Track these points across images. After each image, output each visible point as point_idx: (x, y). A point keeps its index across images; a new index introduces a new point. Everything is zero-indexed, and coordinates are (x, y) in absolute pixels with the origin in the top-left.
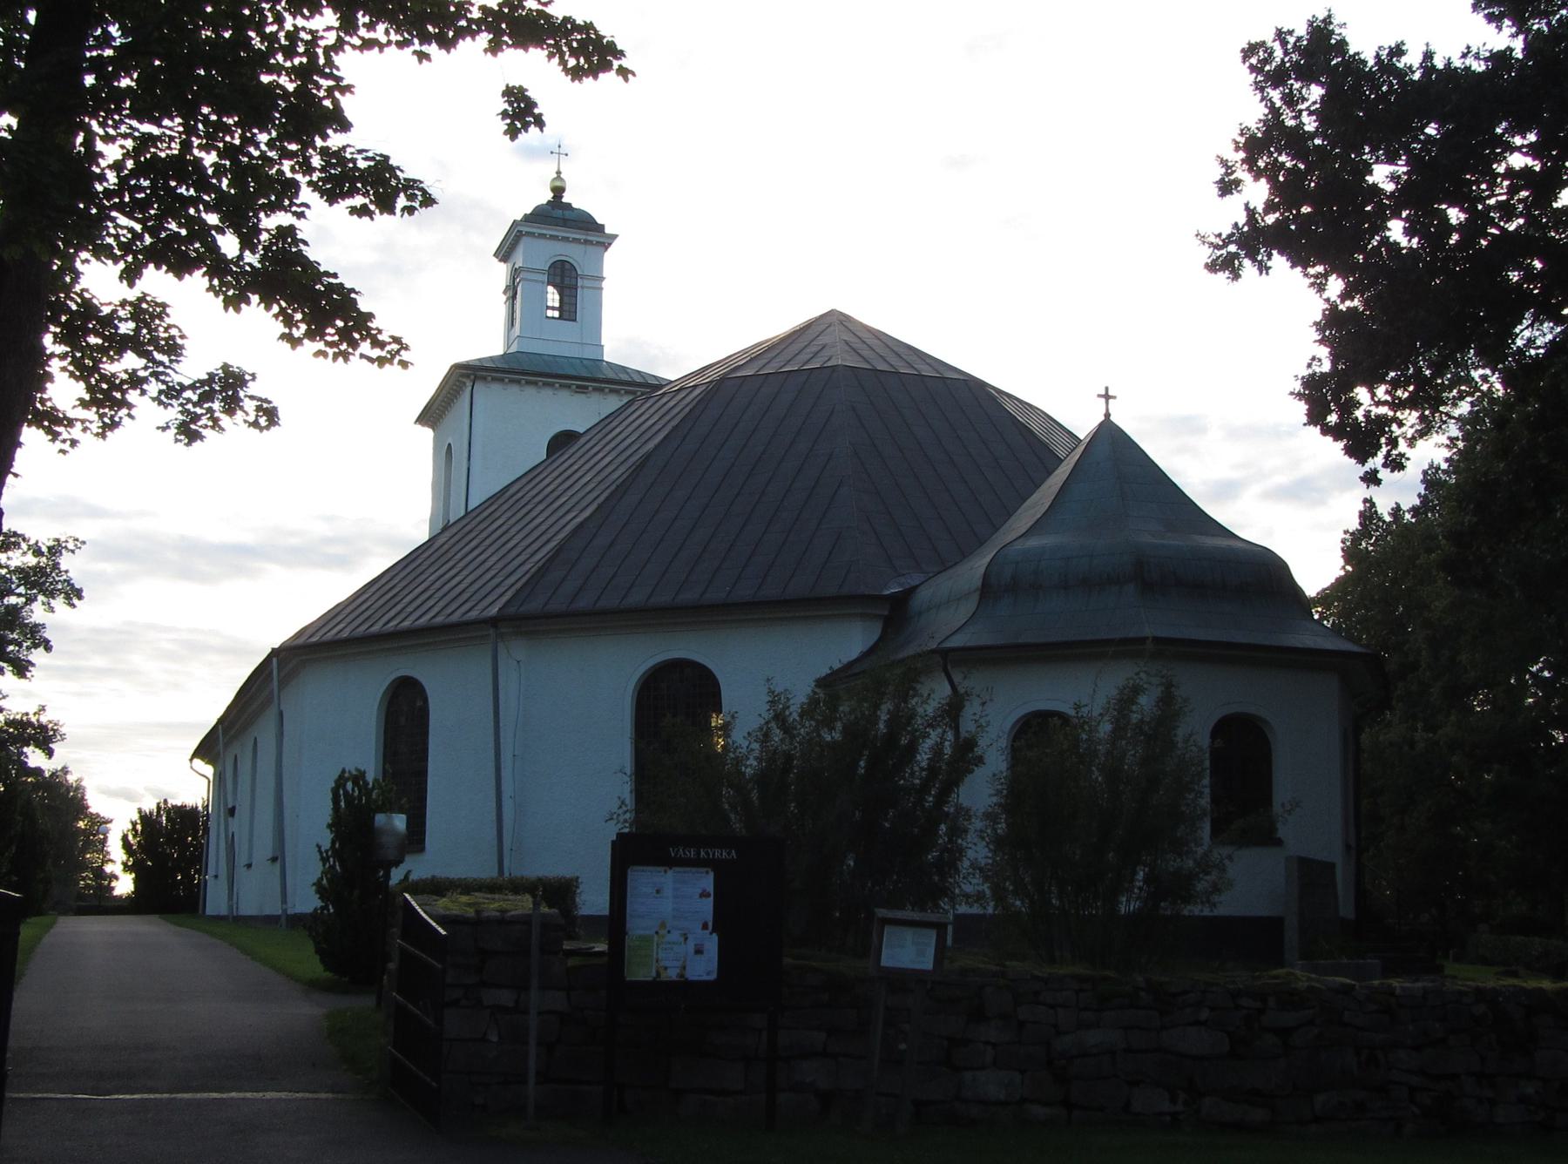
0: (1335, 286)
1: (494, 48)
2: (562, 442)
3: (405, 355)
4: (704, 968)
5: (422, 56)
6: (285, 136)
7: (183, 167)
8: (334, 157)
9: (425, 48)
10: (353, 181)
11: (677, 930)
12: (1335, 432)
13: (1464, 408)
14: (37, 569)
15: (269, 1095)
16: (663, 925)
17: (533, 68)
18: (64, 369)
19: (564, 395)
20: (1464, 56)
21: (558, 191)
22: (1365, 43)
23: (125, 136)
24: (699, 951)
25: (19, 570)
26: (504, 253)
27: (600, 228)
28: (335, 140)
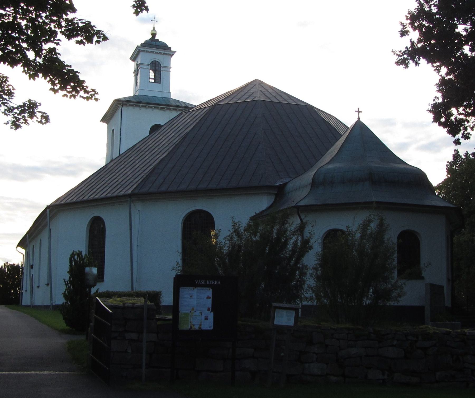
0: (444, 70)
2: (155, 128)
3: (96, 96)
4: (208, 325)
11: (198, 309)
15: (46, 372)
16: (193, 309)
19: (156, 111)
21: (154, 35)
24: (206, 319)
26: (134, 58)
27: (169, 49)
28: (71, 16)
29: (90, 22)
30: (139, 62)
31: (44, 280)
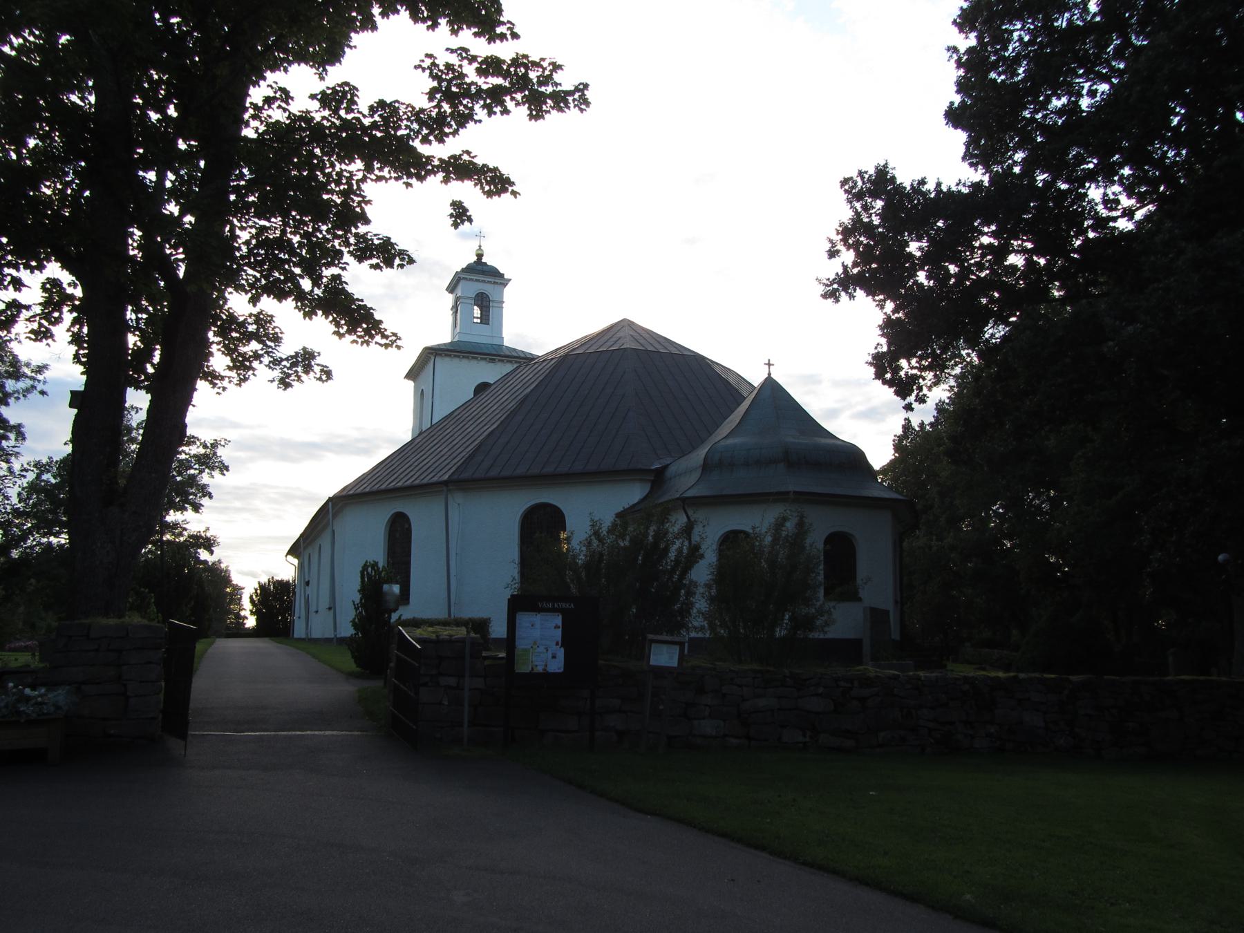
0: (890, 306)
1: (446, 180)
2: (482, 388)
3: (399, 343)
7: (282, 243)
8: (361, 238)
11: (542, 643)
14: (205, 456)
15: (327, 733)
16: (535, 643)
17: (467, 191)
19: (483, 363)
21: (480, 256)
22: (905, 177)
23: (251, 227)
24: (554, 657)
25: (195, 456)
26: (451, 289)
27: (502, 275)
28: (362, 229)
31: (325, 602)
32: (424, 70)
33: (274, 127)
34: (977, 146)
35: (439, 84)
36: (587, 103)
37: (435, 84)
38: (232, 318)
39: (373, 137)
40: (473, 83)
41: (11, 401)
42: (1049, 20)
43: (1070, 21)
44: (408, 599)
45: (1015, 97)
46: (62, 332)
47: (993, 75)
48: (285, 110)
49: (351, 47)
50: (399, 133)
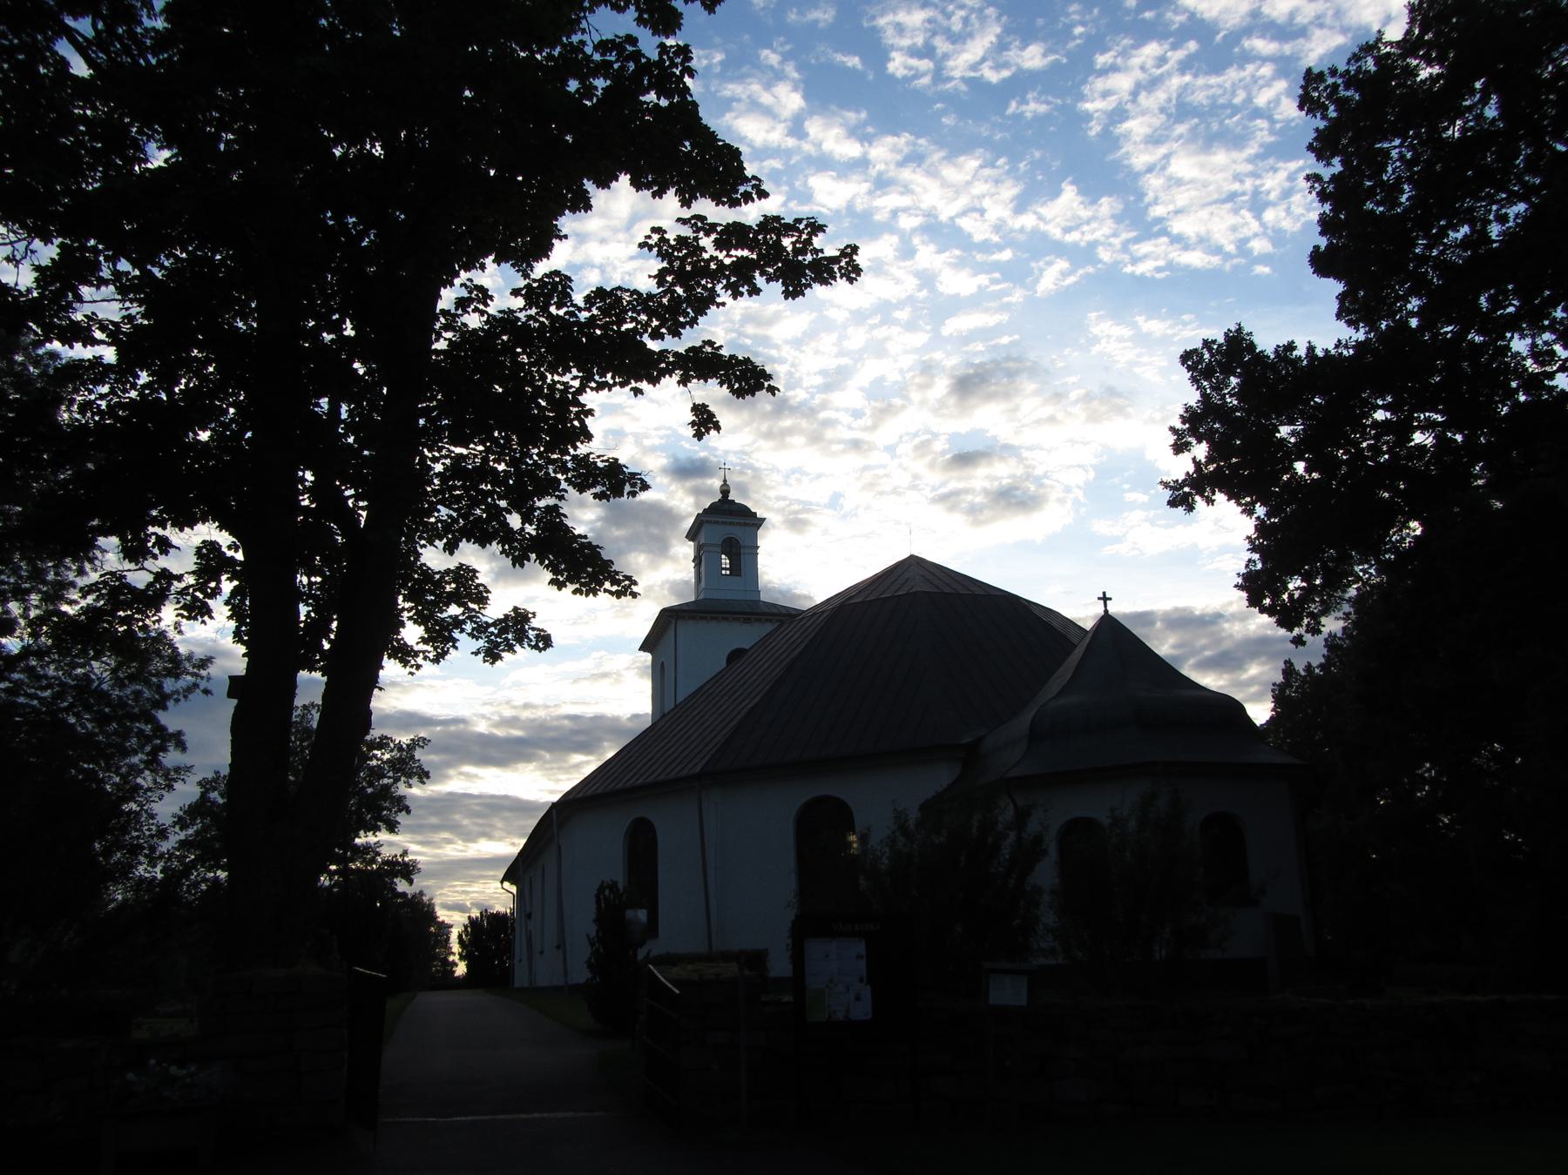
0: (1260, 510)
1: (684, 381)
2: (736, 655)
3: (635, 588)
4: (863, 1010)
5: (637, 392)
6: (550, 448)
7: (485, 472)
8: (583, 462)
9: (639, 385)
10: (595, 477)
11: (841, 978)
12: (1270, 611)
13: (1352, 592)
15: (560, 1115)
17: (711, 392)
18: (410, 618)
20: (1337, 347)
22: (1267, 342)
23: (446, 457)
24: (858, 998)
28: (583, 449)
29: (616, 460)
30: (702, 541)
32: (650, 248)
33: (467, 335)
34: (1355, 300)
35: (670, 263)
36: (857, 270)
37: (665, 264)
38: (427, 573)
39: (591, 336)
40: (712, 258)
41: (170, 704)
42: (1434, 131)
43: (1463, 130)
44: (656, 930)
45: (1397, 231)
46: (220, 608)
47: (1369, 206)
48: (482, 313)
49: (560, 238)
50: (625, 327)
